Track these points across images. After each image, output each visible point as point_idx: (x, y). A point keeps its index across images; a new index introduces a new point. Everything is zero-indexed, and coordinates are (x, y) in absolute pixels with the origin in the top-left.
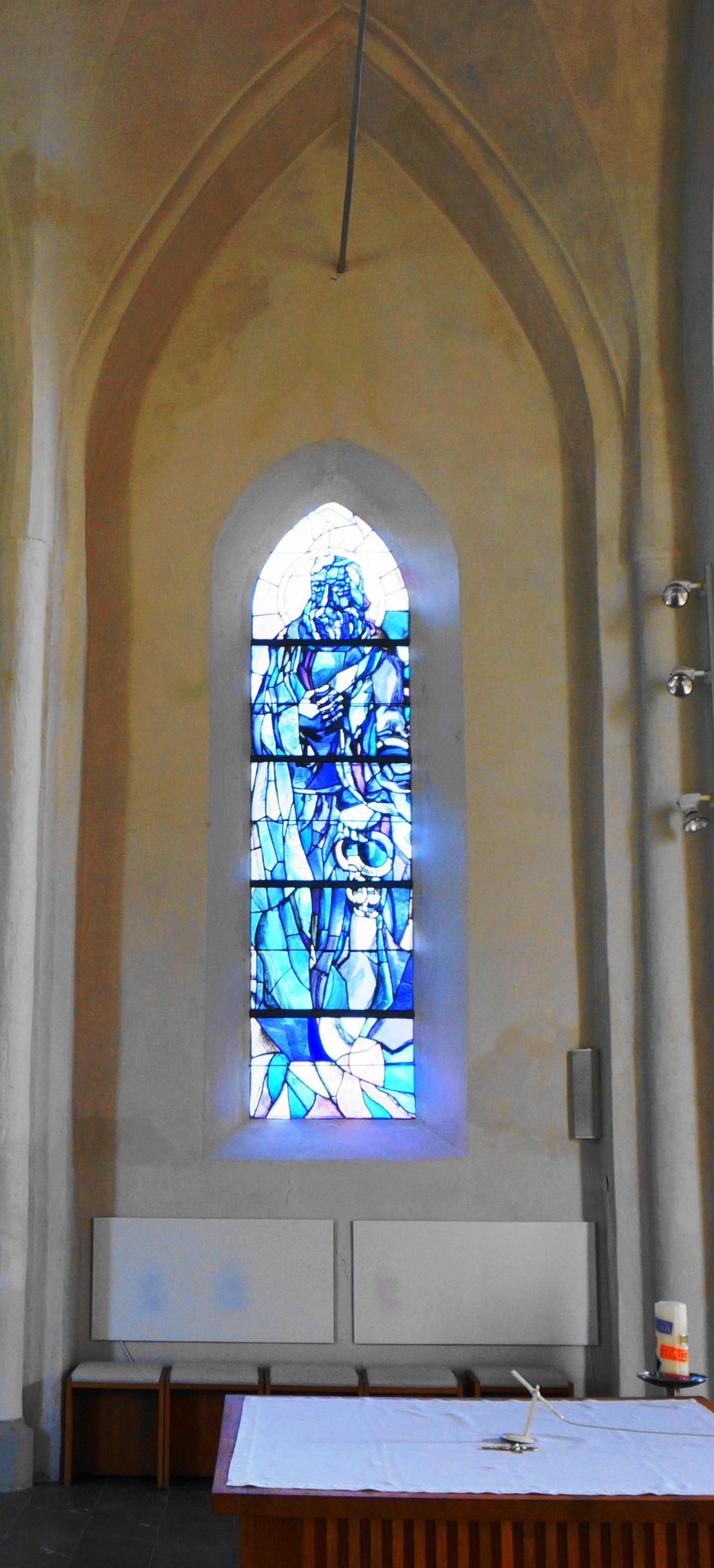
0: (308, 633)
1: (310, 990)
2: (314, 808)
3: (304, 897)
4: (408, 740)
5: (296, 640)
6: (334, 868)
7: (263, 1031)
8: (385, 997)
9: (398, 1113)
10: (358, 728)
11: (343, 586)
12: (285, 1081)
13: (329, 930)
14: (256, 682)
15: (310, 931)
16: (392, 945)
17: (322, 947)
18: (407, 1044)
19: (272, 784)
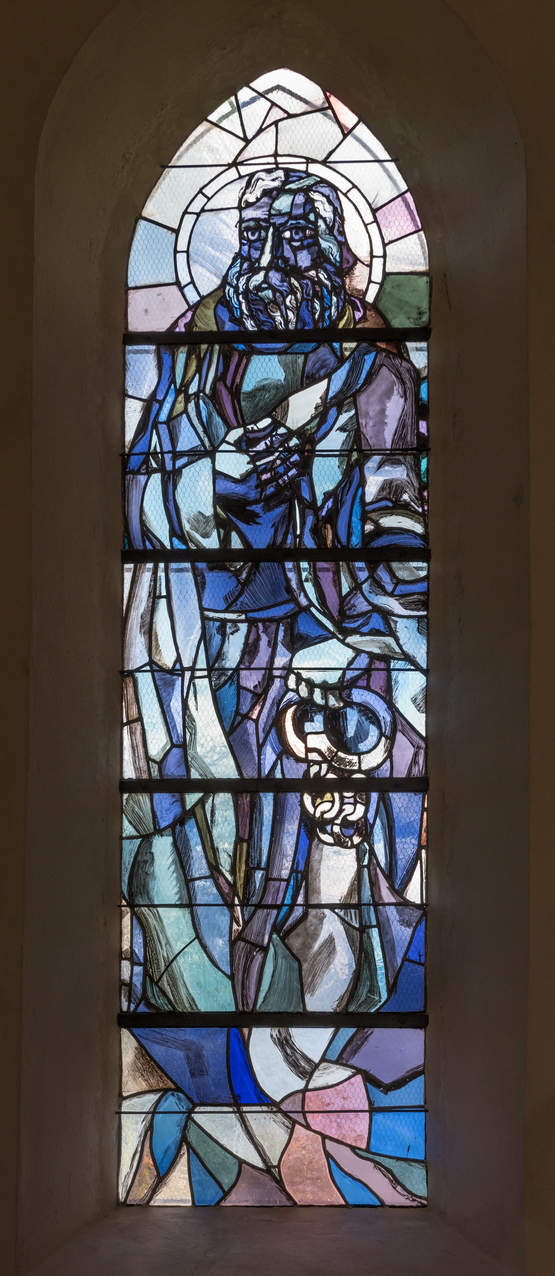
0: (233, 319)
1: (232, 977)
2: (241, 646)
3: (223, 807)
4: (423, 518)
5: (211, 333)
6: (279, 757)
7: (143, 1051)
8: (373, 989)
9: (391, 1196)
10: (328, 496)
11: (303, 229)
12: (184, 1139)
13: (268, 868)
14: (133, 413)
15: (233, 871)
16: (387, 896)
17: (254, 900)
18: (413, 1075)
19: (163, 603)
